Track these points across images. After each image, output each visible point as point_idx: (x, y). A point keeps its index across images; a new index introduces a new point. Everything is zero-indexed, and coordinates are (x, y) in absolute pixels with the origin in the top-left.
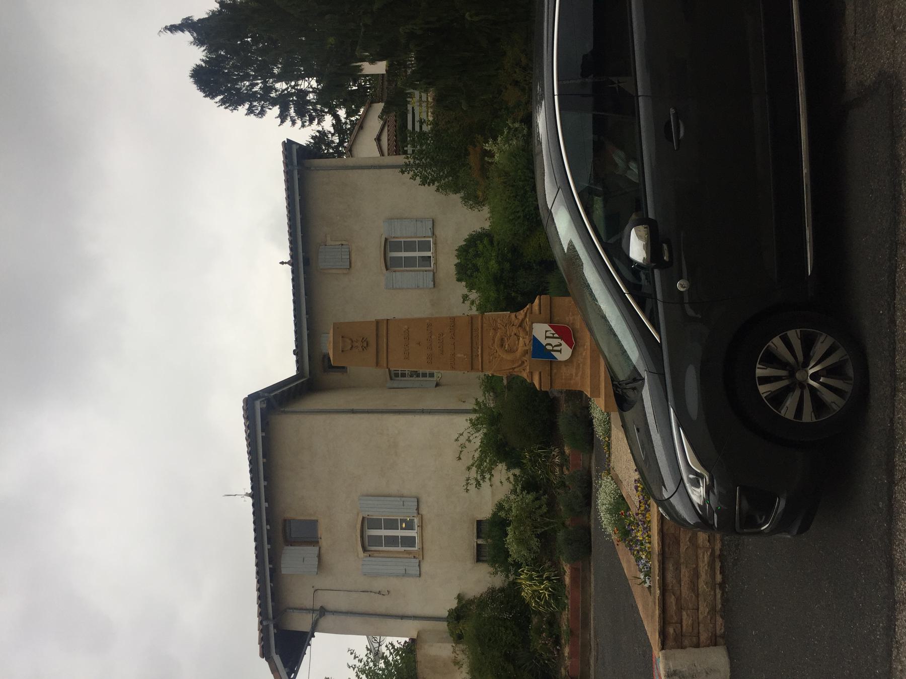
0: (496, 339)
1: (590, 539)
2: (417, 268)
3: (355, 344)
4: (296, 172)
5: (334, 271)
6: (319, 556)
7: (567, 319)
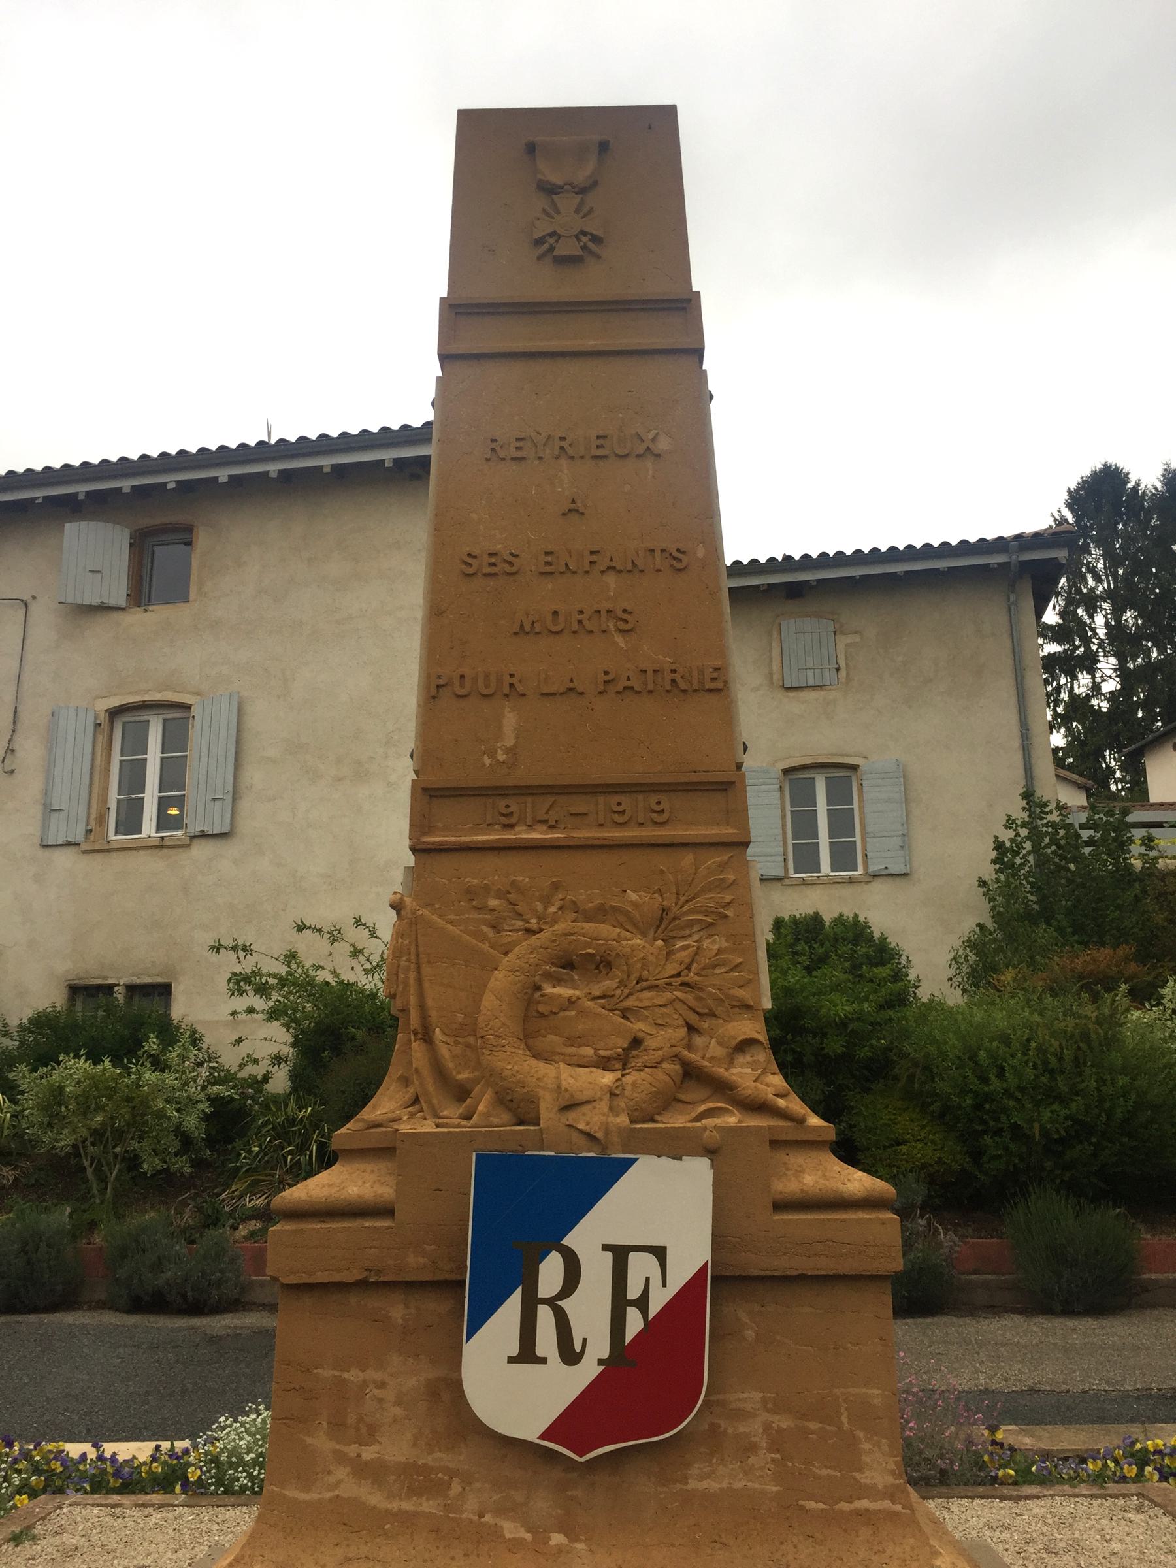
0: (607, 930)
1: (35, 1310)
2: (790, 842)
3: (567, 203)
4: (1002, 558)
5: (776, 652)
6: (104, 608)
7: (750, 1398)
